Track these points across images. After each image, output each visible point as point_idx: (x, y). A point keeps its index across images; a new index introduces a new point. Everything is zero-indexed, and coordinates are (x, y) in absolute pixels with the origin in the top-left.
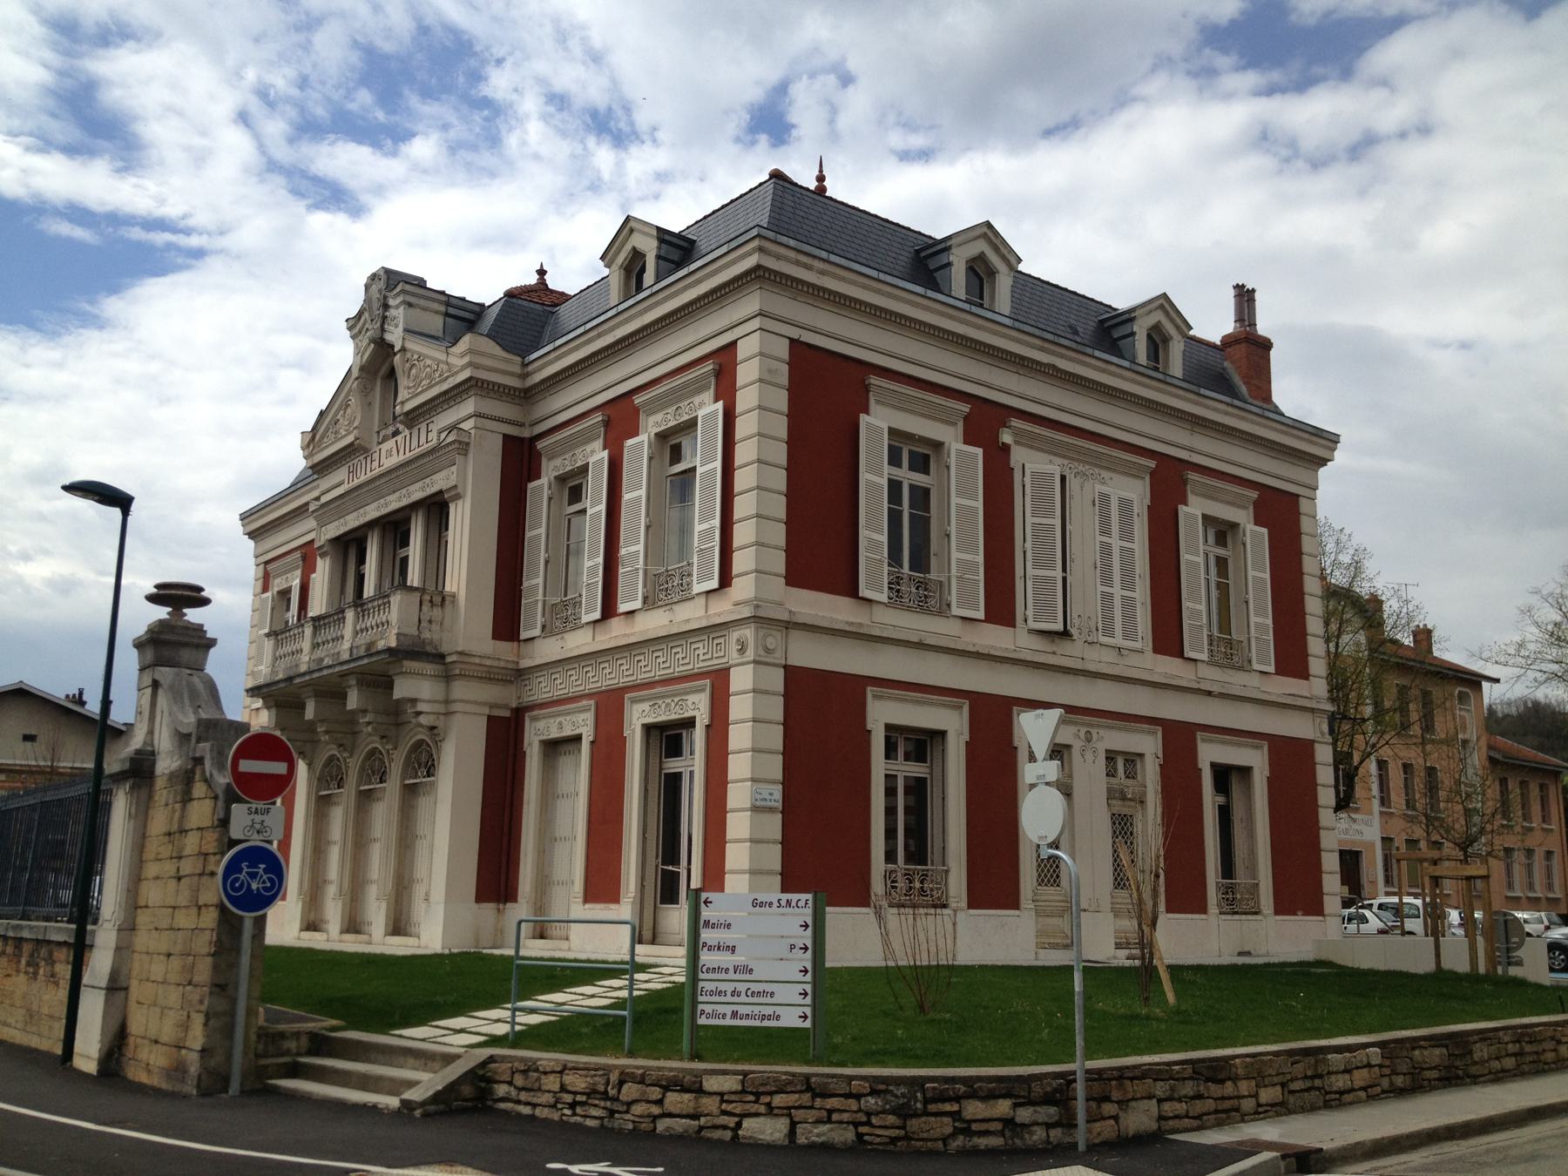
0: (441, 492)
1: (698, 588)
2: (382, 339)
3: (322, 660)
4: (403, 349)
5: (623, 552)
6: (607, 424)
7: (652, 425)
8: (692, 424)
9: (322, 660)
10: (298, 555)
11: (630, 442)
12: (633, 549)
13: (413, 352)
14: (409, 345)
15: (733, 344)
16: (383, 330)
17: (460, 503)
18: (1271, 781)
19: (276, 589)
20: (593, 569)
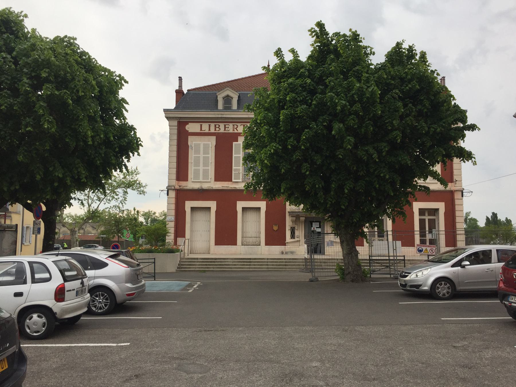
18: (445, 213)
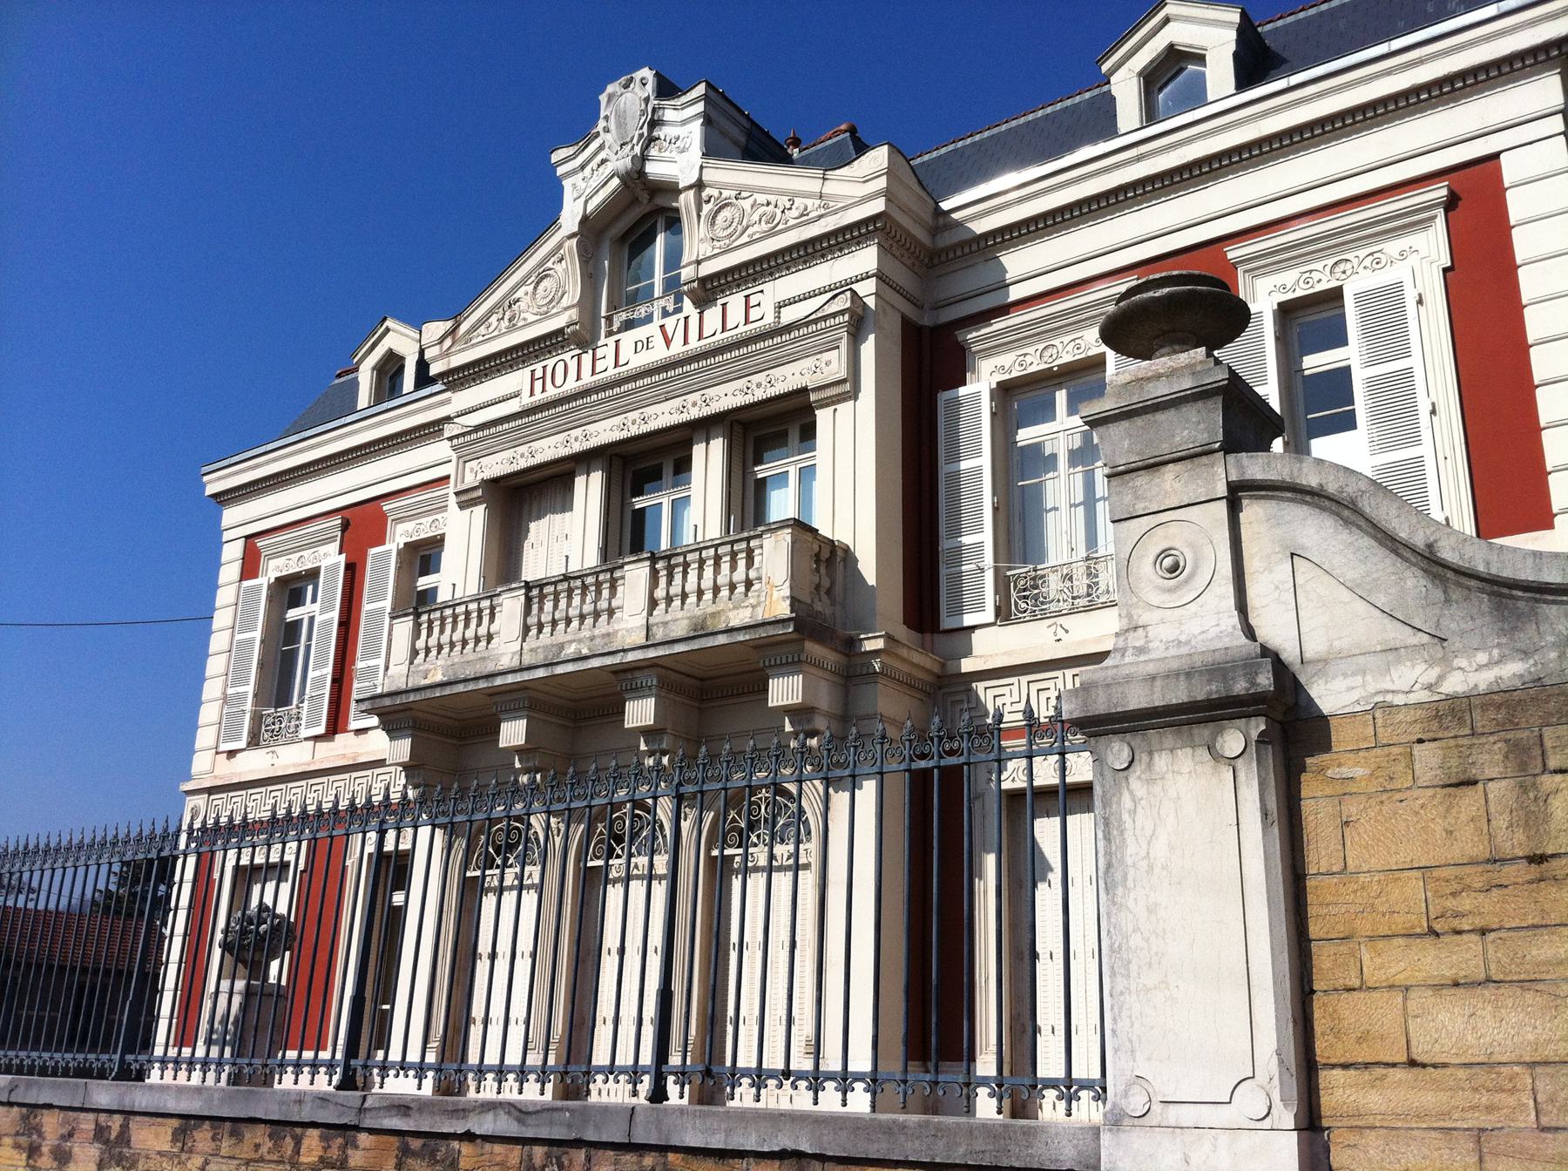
0: (804, 391)
1: (304, 732)
2: (641, 173)
3: (561, 647)
4: (699, 185)
5: (360, 665)
6: (345, 526)
7: (401, 534)
8: (313, 574)
9: (561, 647)
10: (337, 521)
11: (373, 551)
12: (371, 663)
13: (721, 187)
14: (708, 176)
15: (1496, 156)
16: (644, 158)
17: (845, 408)
19: (401, 540)
20: (319, 681)
